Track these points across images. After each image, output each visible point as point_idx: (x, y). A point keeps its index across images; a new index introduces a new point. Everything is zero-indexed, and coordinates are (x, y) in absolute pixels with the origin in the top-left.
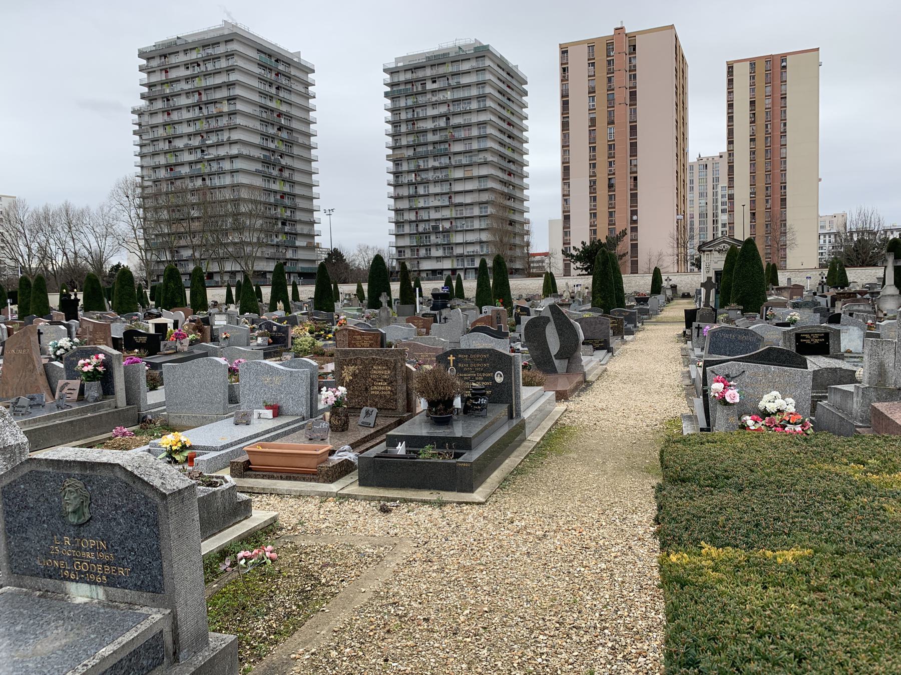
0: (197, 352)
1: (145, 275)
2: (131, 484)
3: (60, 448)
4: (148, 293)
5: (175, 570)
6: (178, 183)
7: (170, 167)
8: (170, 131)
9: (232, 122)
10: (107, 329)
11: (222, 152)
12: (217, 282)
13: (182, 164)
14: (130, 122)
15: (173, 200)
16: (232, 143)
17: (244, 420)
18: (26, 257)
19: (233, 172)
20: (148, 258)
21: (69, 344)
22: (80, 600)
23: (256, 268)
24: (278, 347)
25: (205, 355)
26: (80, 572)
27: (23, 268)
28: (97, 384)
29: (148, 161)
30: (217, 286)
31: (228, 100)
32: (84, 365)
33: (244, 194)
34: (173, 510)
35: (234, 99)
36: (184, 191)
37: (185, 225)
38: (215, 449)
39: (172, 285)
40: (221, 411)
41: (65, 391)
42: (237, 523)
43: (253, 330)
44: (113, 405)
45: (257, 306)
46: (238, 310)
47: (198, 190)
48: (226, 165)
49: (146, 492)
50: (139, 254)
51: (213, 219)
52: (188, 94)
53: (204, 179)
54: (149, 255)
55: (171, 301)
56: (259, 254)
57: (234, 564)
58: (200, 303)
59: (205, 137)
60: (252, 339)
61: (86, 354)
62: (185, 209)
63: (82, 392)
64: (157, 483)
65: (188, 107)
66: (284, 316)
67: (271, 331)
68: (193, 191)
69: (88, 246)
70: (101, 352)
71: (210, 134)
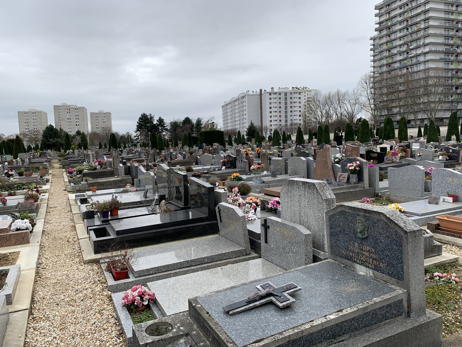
0: (404, 162)
1: (373, 123)
2: (389, 223)
3: (354, 202)
4: (375, 132)
5: (410, 271)
6: (393, 73)
7: (389, 65)
8: (390, 45)
9: (426, 33)
10: (357, 149)
11: (419, 51)
12: (413, 125)
13: (396, 62)
14: (369, 44)
15: (390, 82)
16: (425, 45)
17: (435, 201)
18: (320, 117)
19: (425, 62)
20: (376, 114)
21: (341, 156)
22: (361, 273)
23: (437, 116)
24: (453, 162)
25: (409, 164)
26: (362, 260)
27: (319, 122)
28: (355, 176)
29: (377, 64)
30: (412, 127)
31: (424, 21)
32: (350, 166)
33: (432, 74)
34: (410, 240)
35: (429, 19)
36: (396, 77)
37: (396, 95)
38: (418, 215)
39: (388, 127)
40: (420, 195)
41: (341, 178)
42: (433, 256)
43: (436, 151)
44: (363, 186)
45: (438, 138)
46: (425, 140)
47: (404, 75)
48: (422, 59)
49: (396, 229)
50: (371, 112)
51: (412, 90)
52: (400, 23)
53: (408, 69)
54: (376, 112)
55: (389, 136)
56: (439, 108)
57: (432, 278)
58: (403, 136)
59: (409, 45)
60: (436, 157)
61: (351, 161)
62: (396, 87)
63: (348, 179)
64: (402, 225)
65: (400, 30)
66: (456, 143)
67: (448, 152)
68: (401, 76)
69: (347, 110)
70: (358, 160)
71: (412, 43)
